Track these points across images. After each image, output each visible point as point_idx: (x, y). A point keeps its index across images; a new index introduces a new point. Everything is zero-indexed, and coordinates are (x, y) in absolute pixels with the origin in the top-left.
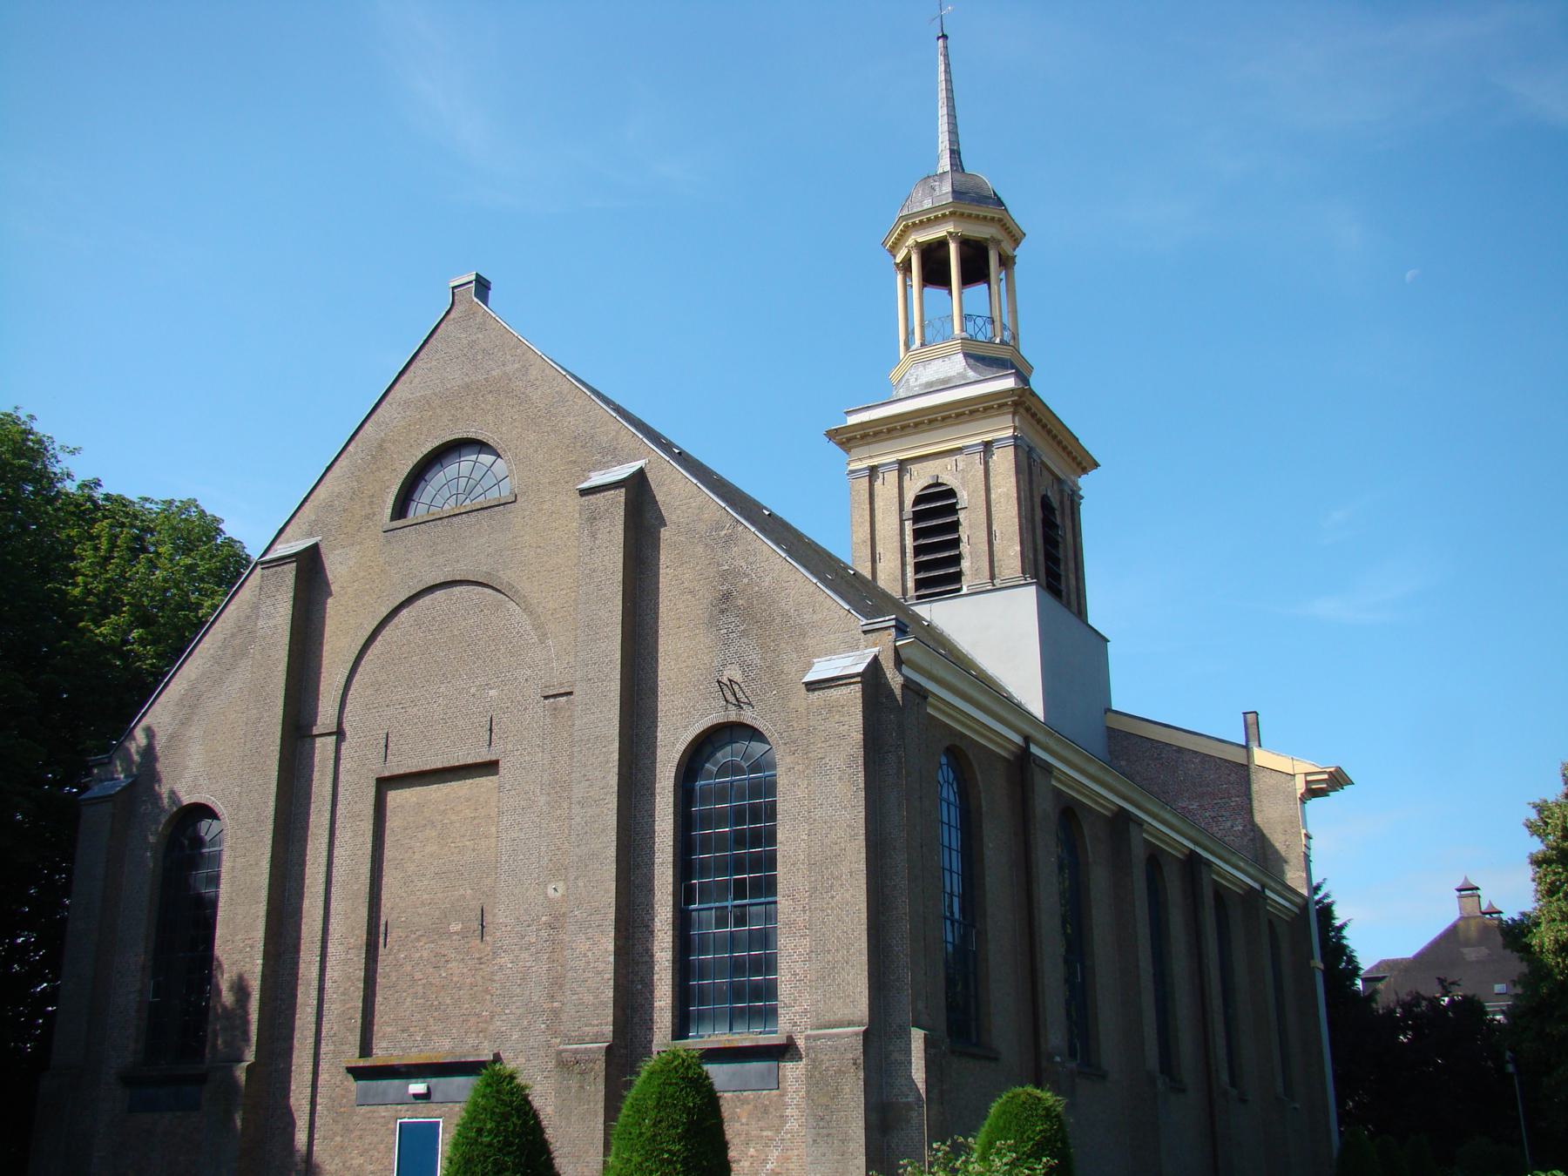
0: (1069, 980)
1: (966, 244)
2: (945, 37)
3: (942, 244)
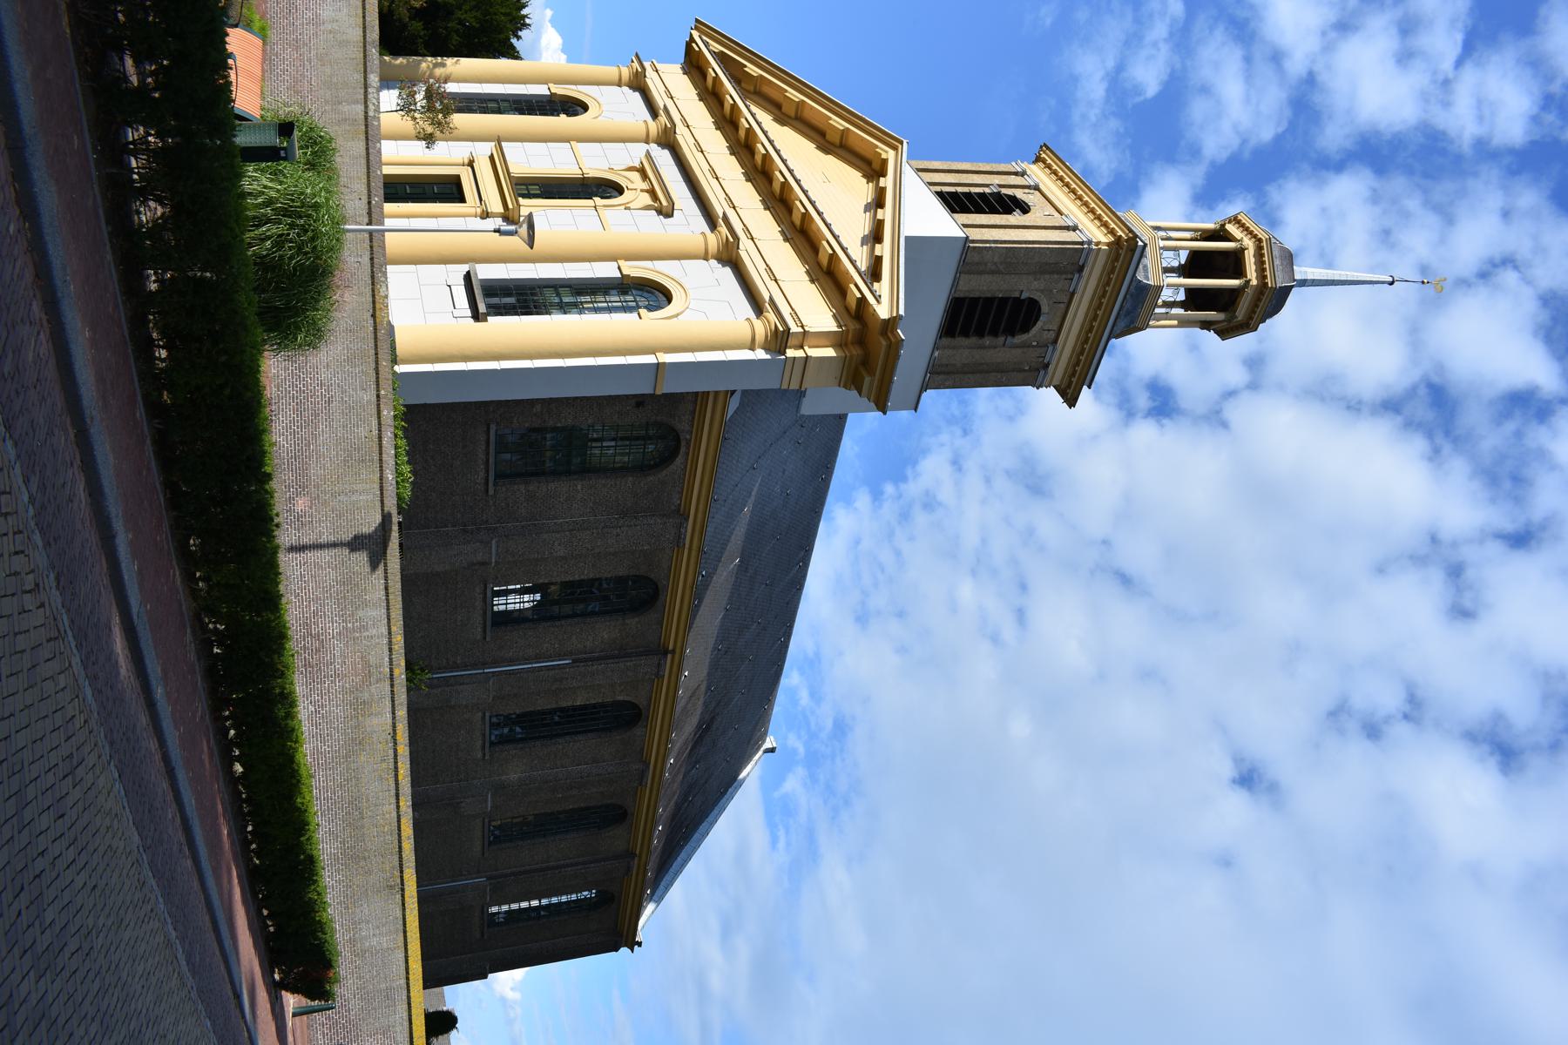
0: (485, 111)
1: (1234, 293)
2: (1391, 283)
3: (1239, 272)
